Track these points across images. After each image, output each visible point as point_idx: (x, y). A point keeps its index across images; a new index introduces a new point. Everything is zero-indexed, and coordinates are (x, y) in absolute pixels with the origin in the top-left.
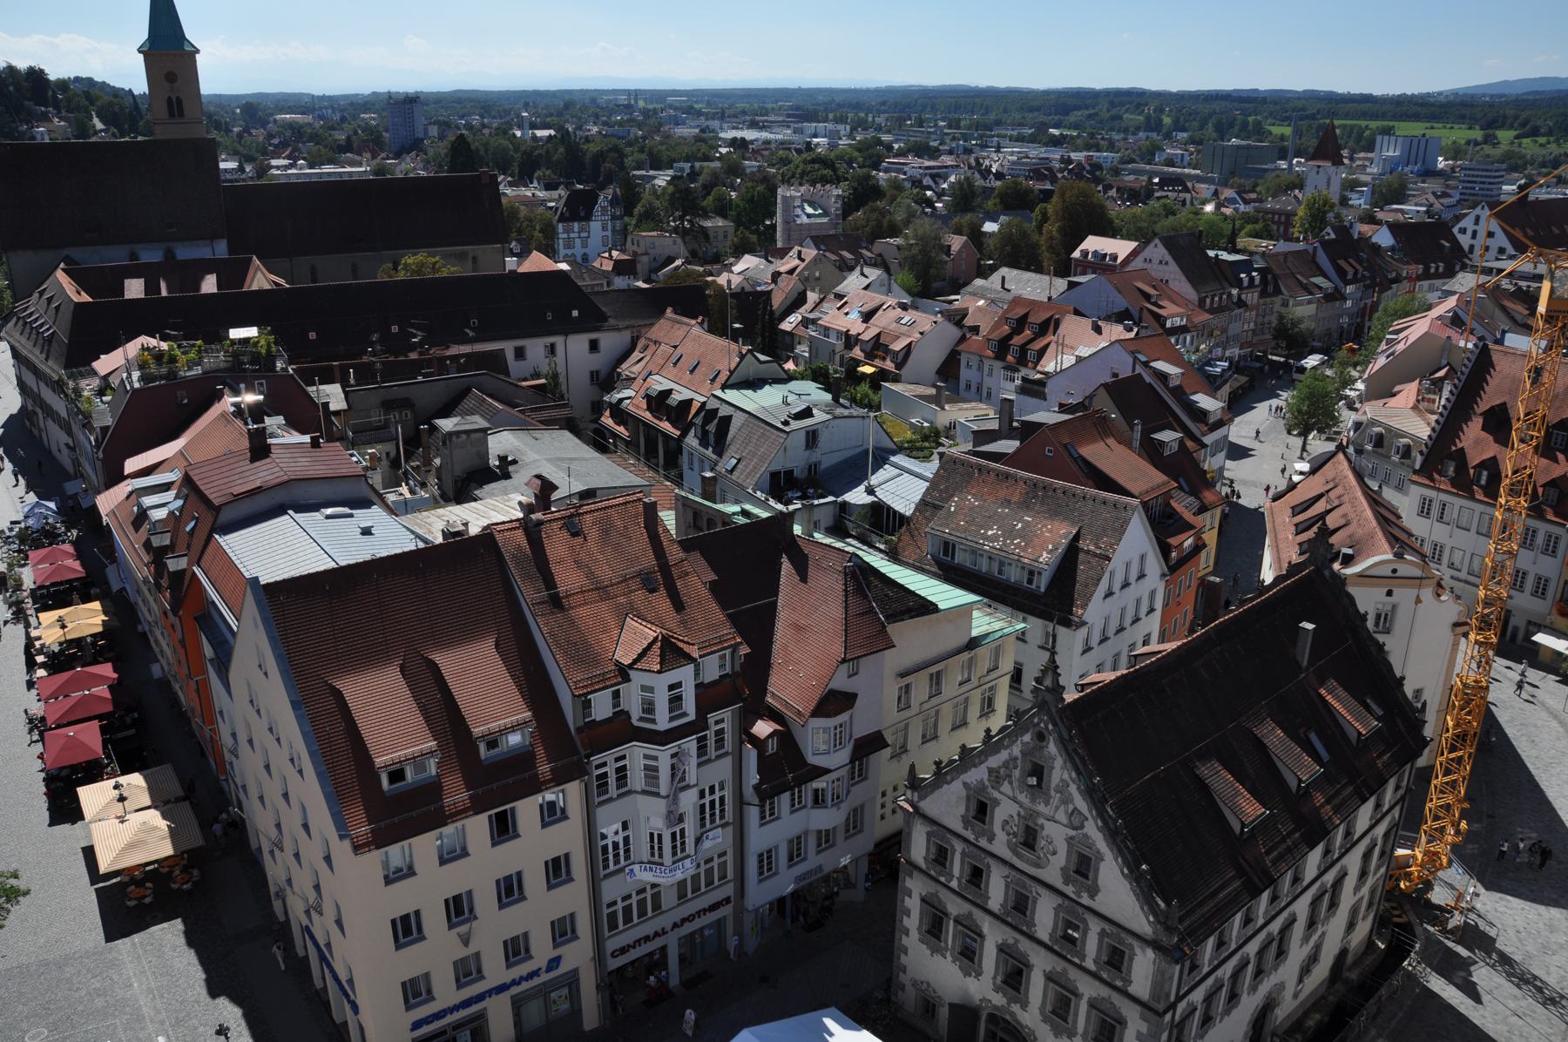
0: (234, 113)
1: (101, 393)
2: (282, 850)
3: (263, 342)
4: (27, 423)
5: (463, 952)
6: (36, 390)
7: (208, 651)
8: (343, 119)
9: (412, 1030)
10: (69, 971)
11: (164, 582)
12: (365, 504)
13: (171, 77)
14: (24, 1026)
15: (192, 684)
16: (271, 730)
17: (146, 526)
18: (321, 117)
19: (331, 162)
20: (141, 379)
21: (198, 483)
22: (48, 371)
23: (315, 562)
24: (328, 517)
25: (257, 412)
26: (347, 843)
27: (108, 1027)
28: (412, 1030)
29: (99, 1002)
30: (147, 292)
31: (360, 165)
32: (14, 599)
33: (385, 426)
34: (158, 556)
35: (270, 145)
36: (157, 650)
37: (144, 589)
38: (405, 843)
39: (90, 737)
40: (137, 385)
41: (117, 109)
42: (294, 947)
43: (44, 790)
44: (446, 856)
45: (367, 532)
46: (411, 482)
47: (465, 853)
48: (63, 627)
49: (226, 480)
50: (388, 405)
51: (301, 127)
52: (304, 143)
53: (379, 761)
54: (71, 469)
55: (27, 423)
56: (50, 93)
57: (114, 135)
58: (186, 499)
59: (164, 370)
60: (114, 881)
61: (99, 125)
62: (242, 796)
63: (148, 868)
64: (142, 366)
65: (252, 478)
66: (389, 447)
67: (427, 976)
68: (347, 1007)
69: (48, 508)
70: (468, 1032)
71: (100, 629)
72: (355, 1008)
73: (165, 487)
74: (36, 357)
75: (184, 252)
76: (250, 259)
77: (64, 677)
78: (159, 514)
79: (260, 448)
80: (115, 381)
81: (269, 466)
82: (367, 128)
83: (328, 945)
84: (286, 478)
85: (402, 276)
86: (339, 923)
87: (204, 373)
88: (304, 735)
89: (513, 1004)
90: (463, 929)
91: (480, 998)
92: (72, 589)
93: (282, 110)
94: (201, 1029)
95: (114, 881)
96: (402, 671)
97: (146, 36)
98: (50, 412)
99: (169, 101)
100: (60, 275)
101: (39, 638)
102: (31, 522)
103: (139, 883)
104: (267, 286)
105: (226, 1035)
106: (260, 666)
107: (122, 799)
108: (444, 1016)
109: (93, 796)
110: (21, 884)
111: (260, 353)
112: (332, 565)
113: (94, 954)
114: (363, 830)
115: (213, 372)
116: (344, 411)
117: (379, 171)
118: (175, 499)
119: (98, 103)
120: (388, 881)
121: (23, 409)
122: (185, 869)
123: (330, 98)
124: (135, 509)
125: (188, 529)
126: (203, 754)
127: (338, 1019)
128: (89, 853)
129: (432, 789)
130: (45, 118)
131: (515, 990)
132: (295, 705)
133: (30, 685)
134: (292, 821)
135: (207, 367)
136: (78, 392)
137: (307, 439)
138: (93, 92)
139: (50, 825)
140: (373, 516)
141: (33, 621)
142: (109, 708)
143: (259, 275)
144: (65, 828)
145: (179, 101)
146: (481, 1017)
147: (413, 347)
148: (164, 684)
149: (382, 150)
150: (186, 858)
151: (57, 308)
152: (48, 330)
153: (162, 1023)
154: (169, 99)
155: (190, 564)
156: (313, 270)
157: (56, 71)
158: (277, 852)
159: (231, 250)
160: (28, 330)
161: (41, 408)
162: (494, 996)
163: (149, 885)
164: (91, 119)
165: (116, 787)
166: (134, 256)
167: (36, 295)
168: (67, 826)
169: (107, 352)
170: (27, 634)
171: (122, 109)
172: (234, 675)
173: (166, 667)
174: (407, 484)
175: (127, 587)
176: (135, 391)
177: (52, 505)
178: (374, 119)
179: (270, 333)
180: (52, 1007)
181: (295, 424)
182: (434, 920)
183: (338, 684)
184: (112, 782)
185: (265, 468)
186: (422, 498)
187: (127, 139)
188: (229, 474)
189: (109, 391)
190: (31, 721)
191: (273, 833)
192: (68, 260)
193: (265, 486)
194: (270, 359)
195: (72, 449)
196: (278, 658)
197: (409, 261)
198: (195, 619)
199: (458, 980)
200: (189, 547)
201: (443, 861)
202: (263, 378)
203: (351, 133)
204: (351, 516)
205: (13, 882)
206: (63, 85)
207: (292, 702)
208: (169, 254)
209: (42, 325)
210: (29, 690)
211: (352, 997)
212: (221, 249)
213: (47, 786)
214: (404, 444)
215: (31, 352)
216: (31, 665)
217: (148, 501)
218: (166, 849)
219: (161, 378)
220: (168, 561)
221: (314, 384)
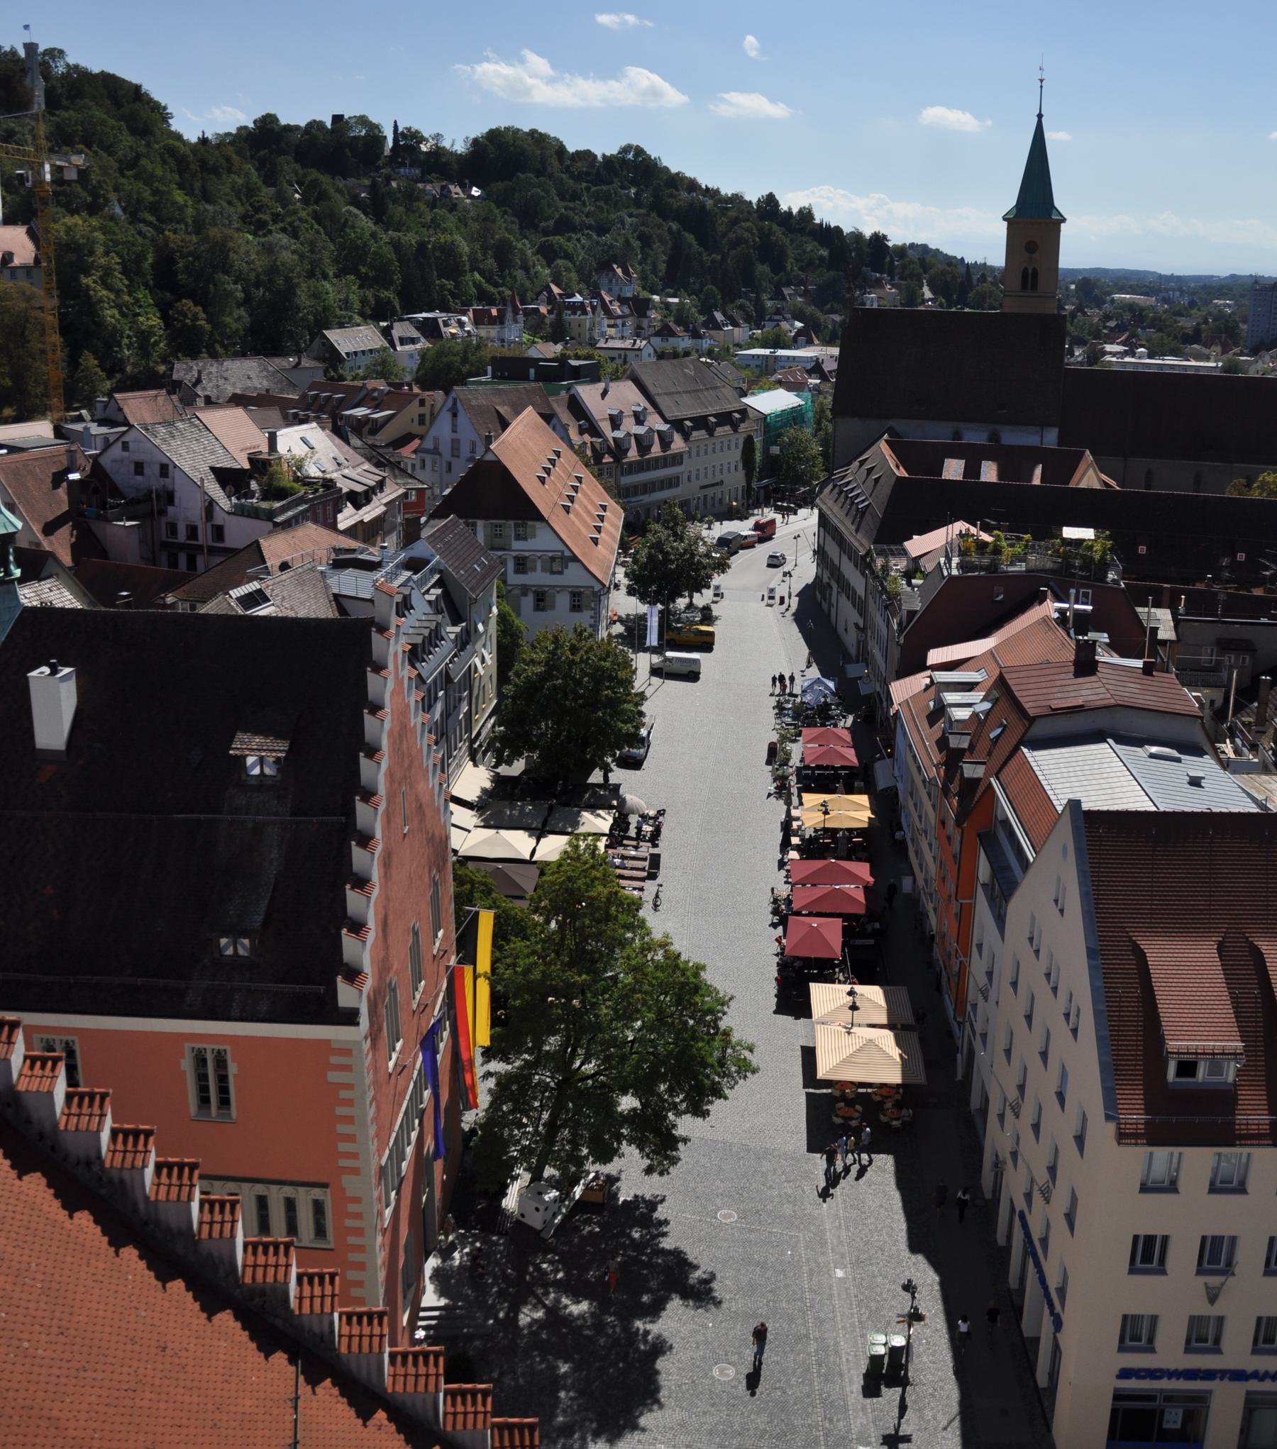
0: (1067, 289)
1: (908, 575)
2: (1017, 1116)
3: (1098, 547)
4: (819, 596)
5: (1203, 1308)
6: (837, 562)
7: (984, 870)
8: (1192, 304)
9: (1119, 1377)
10: (766, 1166)
11: (954, 787)
12: (1199, 752)
13: (1031, 247)
14: (719, 1201)
15: (955, 907)
16: (1048, 975)
17: (941, 725)
18: (1165, 300)
19: (1175, 353)
20: (960, 566)
21: (1014, 688)
22: (856, 544)
23: (1133, 799)
24: (1152, 756)
25: (1082, 623)
26: (1111, 1127)
27: (791, 1237)
28: (1119, 1377)
29: (787, 1209)
30: (965, 475)
31: (1208, 359)
32: (780, 772)
33: (1216, 668)
34: (952, 759)
35: (1105, 327)
36: (915, 862)
37: (923, 793)
38: (1176, 1150)
39: (832, 934)
40: (955, 572)
41: (949, 278)
42: (995, 1232)
43: (776, 975)
44: (1218, 1184)
45: (1195, 782)
46: (1238, 740)
47: (1241, 1189)
48: (826, 813)
49: (1045, 691)
50: (1225, 645)
51: (1142, 309)
52: (1143, 328)
53: (1172, 1044)
54: (853, 651)
55: (819, 596)
56: (888, 259)
57: (941, 305)
58: (995, 702)
59: (986, 561)
60: (824, 1091)
61: (928, 294)
62: (977, 1044)
63: (860, 1090)
64: (962, 553)
65: (1072, 694)
66: (1217, 695)
67: (1154, 1320)
68: (1047, 1319)
69: (827, 687)
70: (1181, 1412)
71: (866, 825)
72: (1058, 1323)
73: (969, 687)
74: (846, 527)
75: (1012, 437)
76: (1084, 452)
77: (818, 864)
78: (962, 714)
79: (1085, 665)
80: (928, 566)
81: (1095, 685)
82: (1220, 316)
83: (1044, 1241)
84: (1112, 702)
85: (1256, 495)
86: (1070, 1218)
87: (1027, 571)
88: (1094, 990)
89: (1247, 1402)
90: (1215, 1280)
91: (1210, 1375)
92: (836, 777)
93: (1122, 290)
94: (879, 1279)
95: (824, 1091)
96: (1219, 950)
97: (1013, 202)
98: (846, 587)
99: (1025, 271)
100: (883, 446)
101: (798, 819)
102: (808, 698)
103: (850, 1103)
104: (1097, 486)
105: (913, 1294)
106: (1056, 901)
107: (854, 1007)
108: (1159, 1378)
109: (826, 997)
110: (754, 1059)
111: (1092, 558)
112: (1154, 809)
113: (792, 1159)
114: (1136, 1117)
115: (1042, 571)
116: (1171, 641)
117: (1231, 367)
118: (982, 701)
119: (932, 271)
120: (1144, 1189)
121: (818, 578)
122: (899, 1105)
123: (1179, 278)
124: (932, 704)
125: (992, 735)
126: (938, 988)
127: (1027, 1329)
128: (809, 1055)
129: (1225, 1099)
130: (878, 284)
131: (1254, 1385)
132: (1091, 953)
133: (781, 864)
134: (1042, 1084)
135: (1032, 565)
136: (886, 569)
137: (1138, 663)
138: (928, 259)
139: (775, 1012)
140: (1203, 766)
141: (795, 800)
142: (862, 911)
143: (1091, 472)
144: (787, 1020)
145: (1035, 273)
146: (1202, 1399)
147: (1261, 582)
148: (913, 901)
149: (1236, 344)
150: (904, 1094)
151: (877, 480)
152: (863, 501)
153: (843, 1256)
154: (1025, 270)
155: (987, 775)
156: (1149, 474)
157: (897, 237)
158: (1009, 1114)
159: (1062, 440)
160: (842, 499)
161: (838, 582)
162: (1226, 1381)
163: (858, 1107)
164: (921, 287)
165: (851, 993)
166: (957, 435)
167: (856, 464)
168: (790, 1019)
169: (920, 533)
170: (788, 812)
171: (954, 277)
172: (1017, 907)
173: (921, 882)
174: (1232, 742)
175: (900, 786)
176: (951, 577)
177: (831, 685)
178: (1229, 306)
179: (1107, 538)
180: (745, 1195)
181: (1118, 647)
182: (1182, 1256)
183: (1144, 944)
184: (847, 988)
185: (1089, 686)
186: (1249, 762)
187: (954, 310)
188: (1048, 684)
189: (918, 575)
190: (775, 901)
191: (1013, 1094)
192: (892, 432)
193: (1087, 706)
194: (1104, 566)
195: (861, 630)
196: (1084, 896)
197: (1268, 479)
198: (979, 836)
199: (1188, 1341)
200: (990, 754)
201: (1213, 1189)
202: (1088, 587)
203: (1200, 320)
204: (1178, 760)
205: (746, 1053)
206: (902, 251)
207: (1088, 949)
208: (994, 437)
209: (857, 496)
210: (779, 870)
211: (1058, 1308)
212: (1050, 438)
213: (779, 971)
214: (1237, 693)
215: (841, 521)
216: (785, 845)
217: (950, 697)
218: (893, 1076)
219: (981, 568)
220: (965, 766)
221: (1146, 605)
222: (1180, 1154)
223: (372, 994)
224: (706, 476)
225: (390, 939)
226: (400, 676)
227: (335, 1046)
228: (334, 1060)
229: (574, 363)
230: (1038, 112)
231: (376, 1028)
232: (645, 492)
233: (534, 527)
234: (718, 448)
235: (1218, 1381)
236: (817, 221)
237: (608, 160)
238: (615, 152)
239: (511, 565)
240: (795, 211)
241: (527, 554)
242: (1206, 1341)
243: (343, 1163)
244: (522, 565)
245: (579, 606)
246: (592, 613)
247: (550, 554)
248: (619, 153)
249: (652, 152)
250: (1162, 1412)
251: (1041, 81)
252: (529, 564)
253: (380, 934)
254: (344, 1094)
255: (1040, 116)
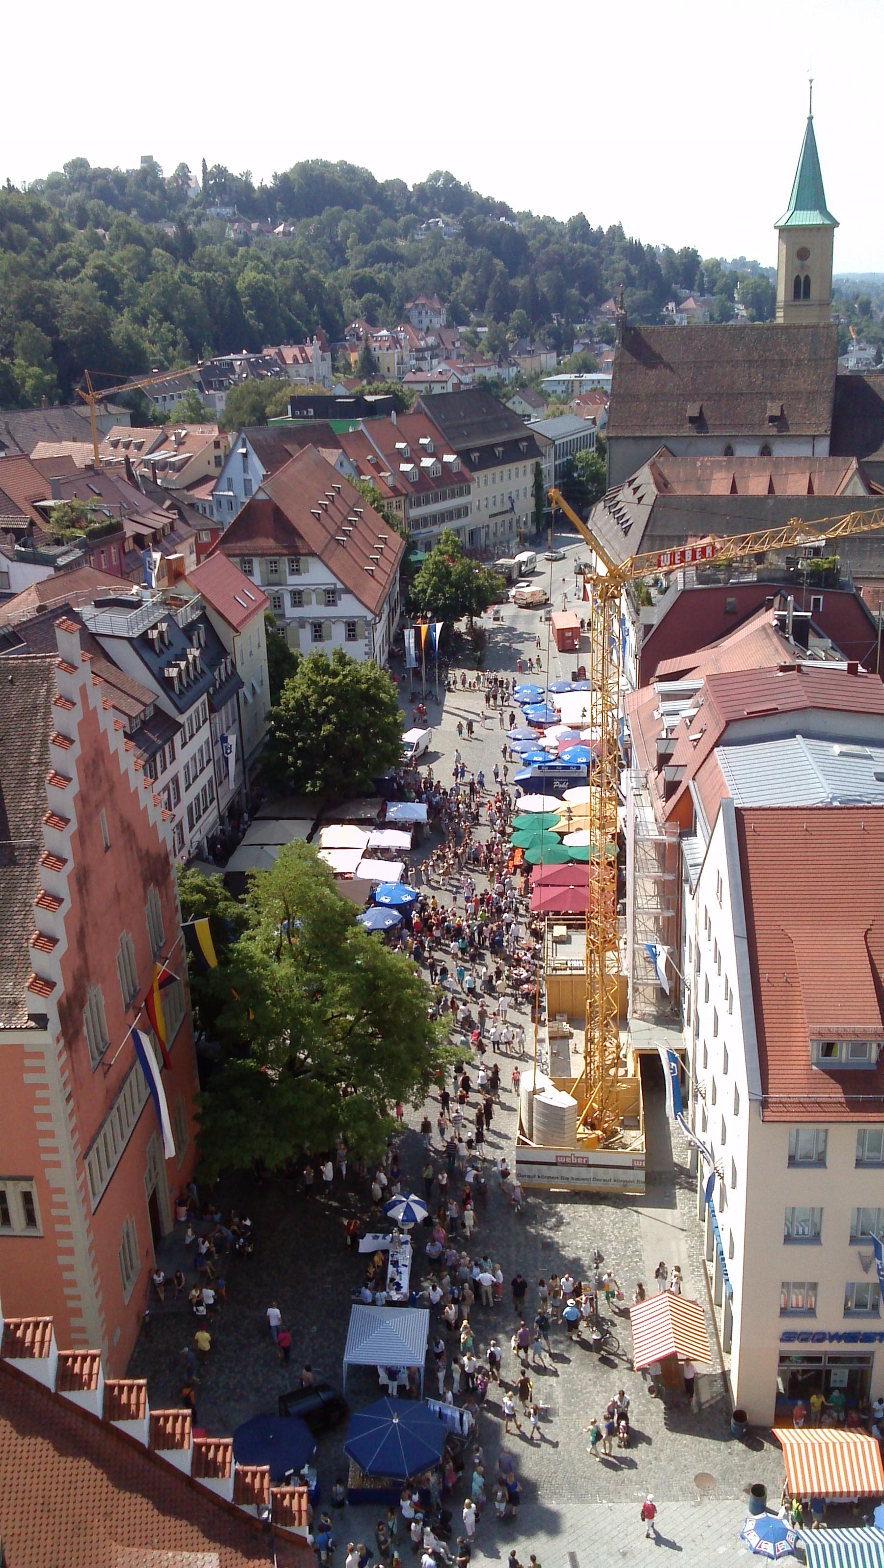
9: (782, 1340)
28: (782, 1340)
70: (847, 1372)
91: (868, 1338)
99: (797, 280)
154: (798, 277)
204: (869, 758)
222: (798, 1131)
223: (64, 1001)
224: (494, 504)
225: (89, 950)
226: (91, 707)
227: (27, 1050)
228: (28, 1063)
229: (370, 398)
230: (808, 115)
231: (71, 1031)
232: (434, 523)
233: (307, 562)
234: (505, 476)
235: (877, 1342)
236: (627, 237)
237: (420, 189)
238: (424, 180)
239: (287, 600)
240: (605, 230)
241: (301, 588)
242: (865, 1306)
243: (45, 1157)
244: (298, 599)
245: (320, 636)
246: (366, 641)
247: (324, 587)
248: (429, 181)
249: (462, 179)
250: (828, 1373)
251: (811, 81)
252: (304, 598)
253: (75, 945)
254: (40, 1094)
255: (810, 119)
